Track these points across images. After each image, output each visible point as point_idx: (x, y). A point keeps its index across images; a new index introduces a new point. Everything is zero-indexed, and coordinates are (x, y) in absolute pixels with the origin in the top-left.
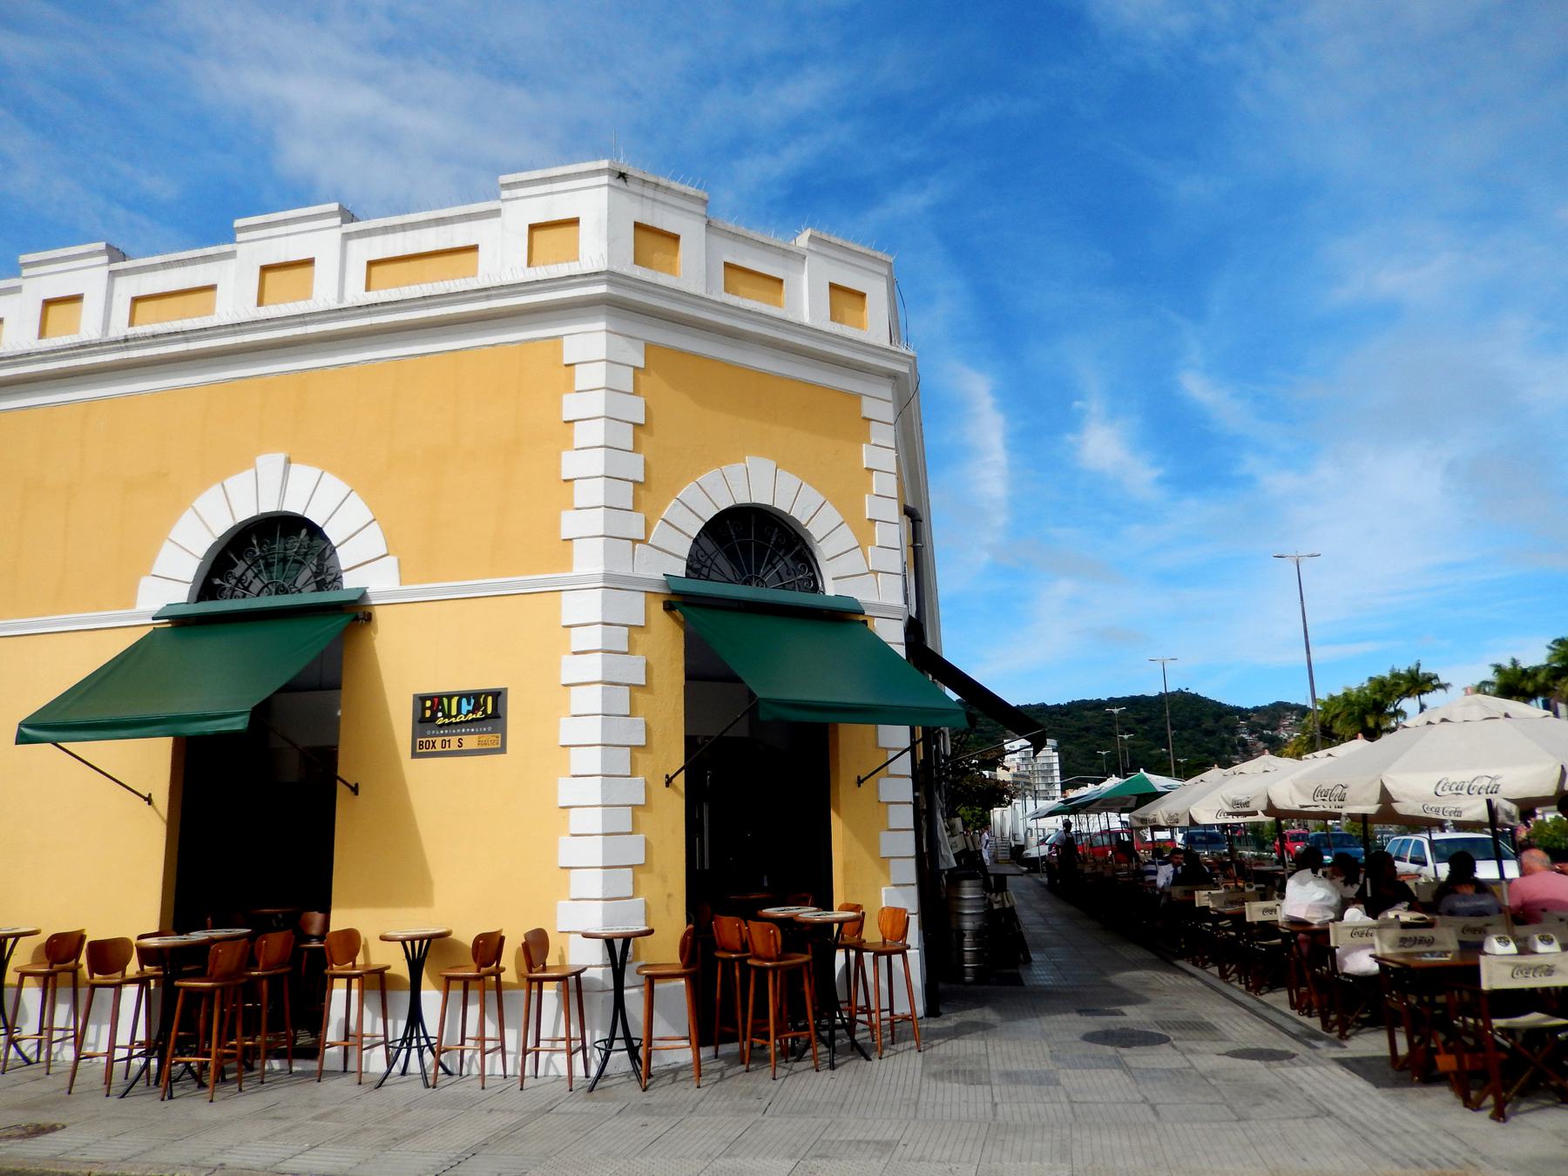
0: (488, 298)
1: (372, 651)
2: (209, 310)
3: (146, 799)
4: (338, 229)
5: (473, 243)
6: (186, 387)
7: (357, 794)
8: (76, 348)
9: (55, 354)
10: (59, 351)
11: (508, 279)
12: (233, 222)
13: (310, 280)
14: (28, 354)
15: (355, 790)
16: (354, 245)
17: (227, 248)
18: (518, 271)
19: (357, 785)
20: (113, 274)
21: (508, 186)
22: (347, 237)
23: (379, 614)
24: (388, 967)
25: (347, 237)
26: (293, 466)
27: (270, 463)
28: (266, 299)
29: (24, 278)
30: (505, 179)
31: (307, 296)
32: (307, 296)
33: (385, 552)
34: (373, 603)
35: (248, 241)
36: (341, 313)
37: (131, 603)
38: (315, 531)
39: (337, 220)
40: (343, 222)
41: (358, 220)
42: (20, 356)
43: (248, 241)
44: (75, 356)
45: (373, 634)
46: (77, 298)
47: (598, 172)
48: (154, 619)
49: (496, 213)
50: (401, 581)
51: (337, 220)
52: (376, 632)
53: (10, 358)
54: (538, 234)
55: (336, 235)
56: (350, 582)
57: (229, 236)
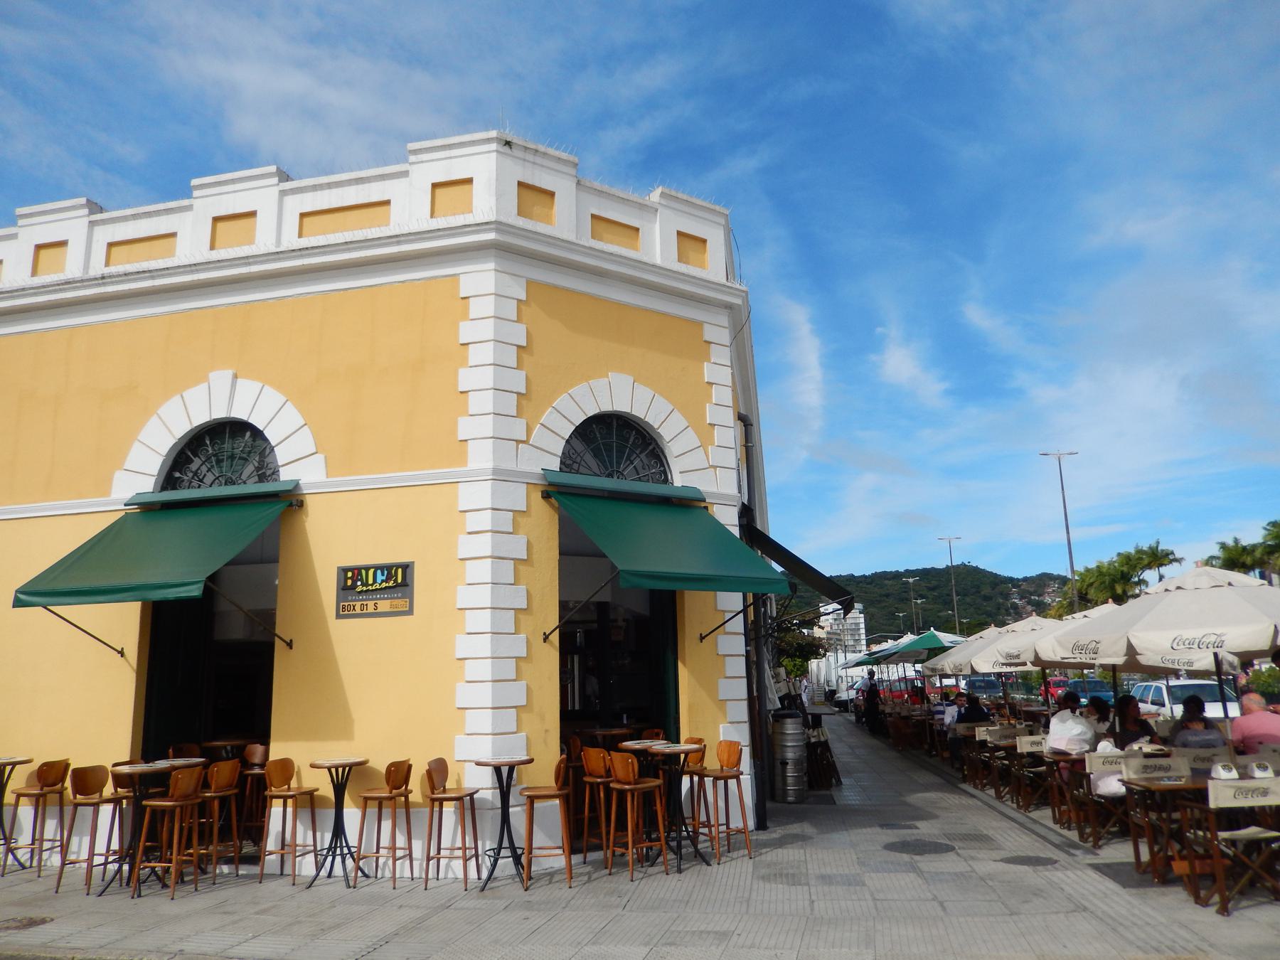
0: (399, 243)
1: (303, 532)
2: (171, 253)
3: (119, 652)
4: (276, 187)
5: (386, 199)
6: (152, 316)
7: (291, 648)
8: (62, 284)
9: (46, 289)
10: (48, 286)
11: (415, 228)
12: (406, 145)
13: (253, 229)
14: (23, 289)
15: (290, 645)
16: (289, 200)
17: (185, 202)
18: (422, 221)
19: (291, 641)
20: (92, 224)
21: (415, 152)
22: (283, 193)
23: (309, 501)
24: (317, 790)
25: (283, 193)
26: (239, 381)
27: (220, 378)
28: (435, 214)
29: (20, 227)
30: (412, 146)
31: (251, 242)
32: (251, 242)
33: (315, 451)
34: (305, 492)
35: (202, 197)
36: (278, 255)
37: (107, 492)
38: (257, 434)
39: (275, 180)
40: (280, 181)
41: (292, 180)
42: (17, 291)
43: (202, 197)
44: (61, 290)
45: (304, 517)
46: (63, 244)
47: (488, 141)
48: (125, 505)
49: (405, 174)
50: (327, 474)
51: (275, 180)
52: (307, 516)
53: (8, 292)
54: (220, 225)
55: (274, 192)
56: (286, 475)
57: (187, 192)
